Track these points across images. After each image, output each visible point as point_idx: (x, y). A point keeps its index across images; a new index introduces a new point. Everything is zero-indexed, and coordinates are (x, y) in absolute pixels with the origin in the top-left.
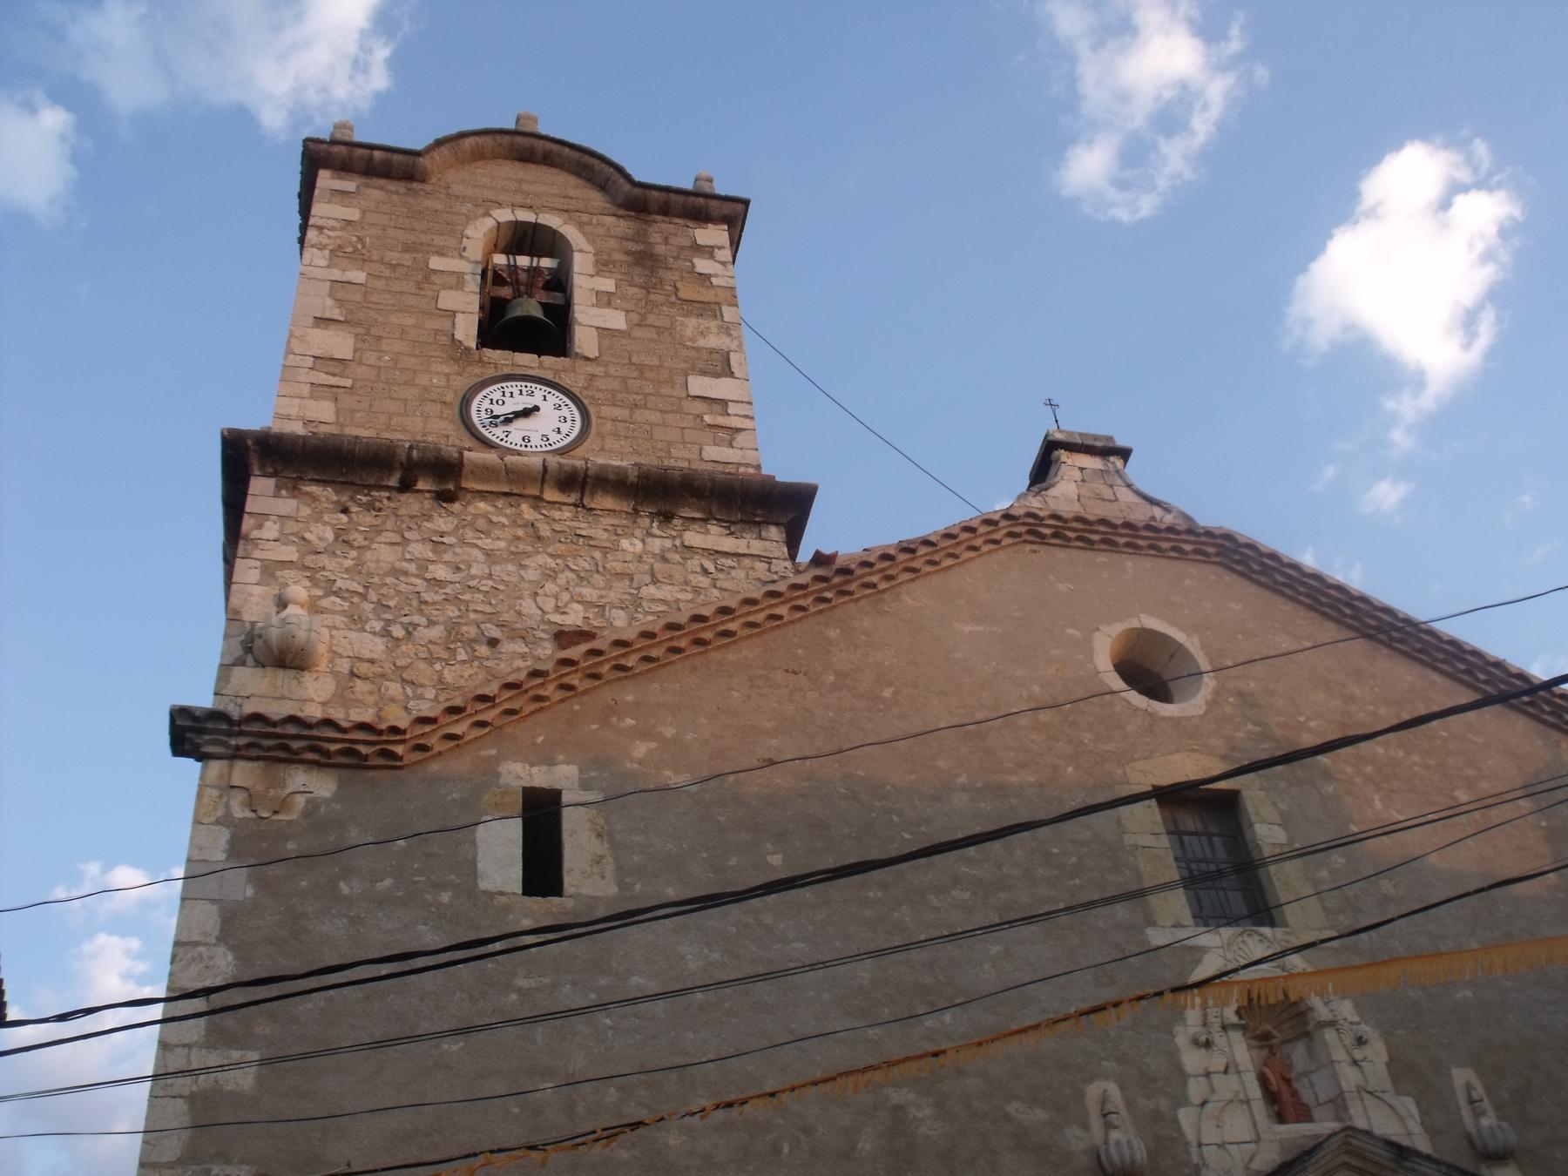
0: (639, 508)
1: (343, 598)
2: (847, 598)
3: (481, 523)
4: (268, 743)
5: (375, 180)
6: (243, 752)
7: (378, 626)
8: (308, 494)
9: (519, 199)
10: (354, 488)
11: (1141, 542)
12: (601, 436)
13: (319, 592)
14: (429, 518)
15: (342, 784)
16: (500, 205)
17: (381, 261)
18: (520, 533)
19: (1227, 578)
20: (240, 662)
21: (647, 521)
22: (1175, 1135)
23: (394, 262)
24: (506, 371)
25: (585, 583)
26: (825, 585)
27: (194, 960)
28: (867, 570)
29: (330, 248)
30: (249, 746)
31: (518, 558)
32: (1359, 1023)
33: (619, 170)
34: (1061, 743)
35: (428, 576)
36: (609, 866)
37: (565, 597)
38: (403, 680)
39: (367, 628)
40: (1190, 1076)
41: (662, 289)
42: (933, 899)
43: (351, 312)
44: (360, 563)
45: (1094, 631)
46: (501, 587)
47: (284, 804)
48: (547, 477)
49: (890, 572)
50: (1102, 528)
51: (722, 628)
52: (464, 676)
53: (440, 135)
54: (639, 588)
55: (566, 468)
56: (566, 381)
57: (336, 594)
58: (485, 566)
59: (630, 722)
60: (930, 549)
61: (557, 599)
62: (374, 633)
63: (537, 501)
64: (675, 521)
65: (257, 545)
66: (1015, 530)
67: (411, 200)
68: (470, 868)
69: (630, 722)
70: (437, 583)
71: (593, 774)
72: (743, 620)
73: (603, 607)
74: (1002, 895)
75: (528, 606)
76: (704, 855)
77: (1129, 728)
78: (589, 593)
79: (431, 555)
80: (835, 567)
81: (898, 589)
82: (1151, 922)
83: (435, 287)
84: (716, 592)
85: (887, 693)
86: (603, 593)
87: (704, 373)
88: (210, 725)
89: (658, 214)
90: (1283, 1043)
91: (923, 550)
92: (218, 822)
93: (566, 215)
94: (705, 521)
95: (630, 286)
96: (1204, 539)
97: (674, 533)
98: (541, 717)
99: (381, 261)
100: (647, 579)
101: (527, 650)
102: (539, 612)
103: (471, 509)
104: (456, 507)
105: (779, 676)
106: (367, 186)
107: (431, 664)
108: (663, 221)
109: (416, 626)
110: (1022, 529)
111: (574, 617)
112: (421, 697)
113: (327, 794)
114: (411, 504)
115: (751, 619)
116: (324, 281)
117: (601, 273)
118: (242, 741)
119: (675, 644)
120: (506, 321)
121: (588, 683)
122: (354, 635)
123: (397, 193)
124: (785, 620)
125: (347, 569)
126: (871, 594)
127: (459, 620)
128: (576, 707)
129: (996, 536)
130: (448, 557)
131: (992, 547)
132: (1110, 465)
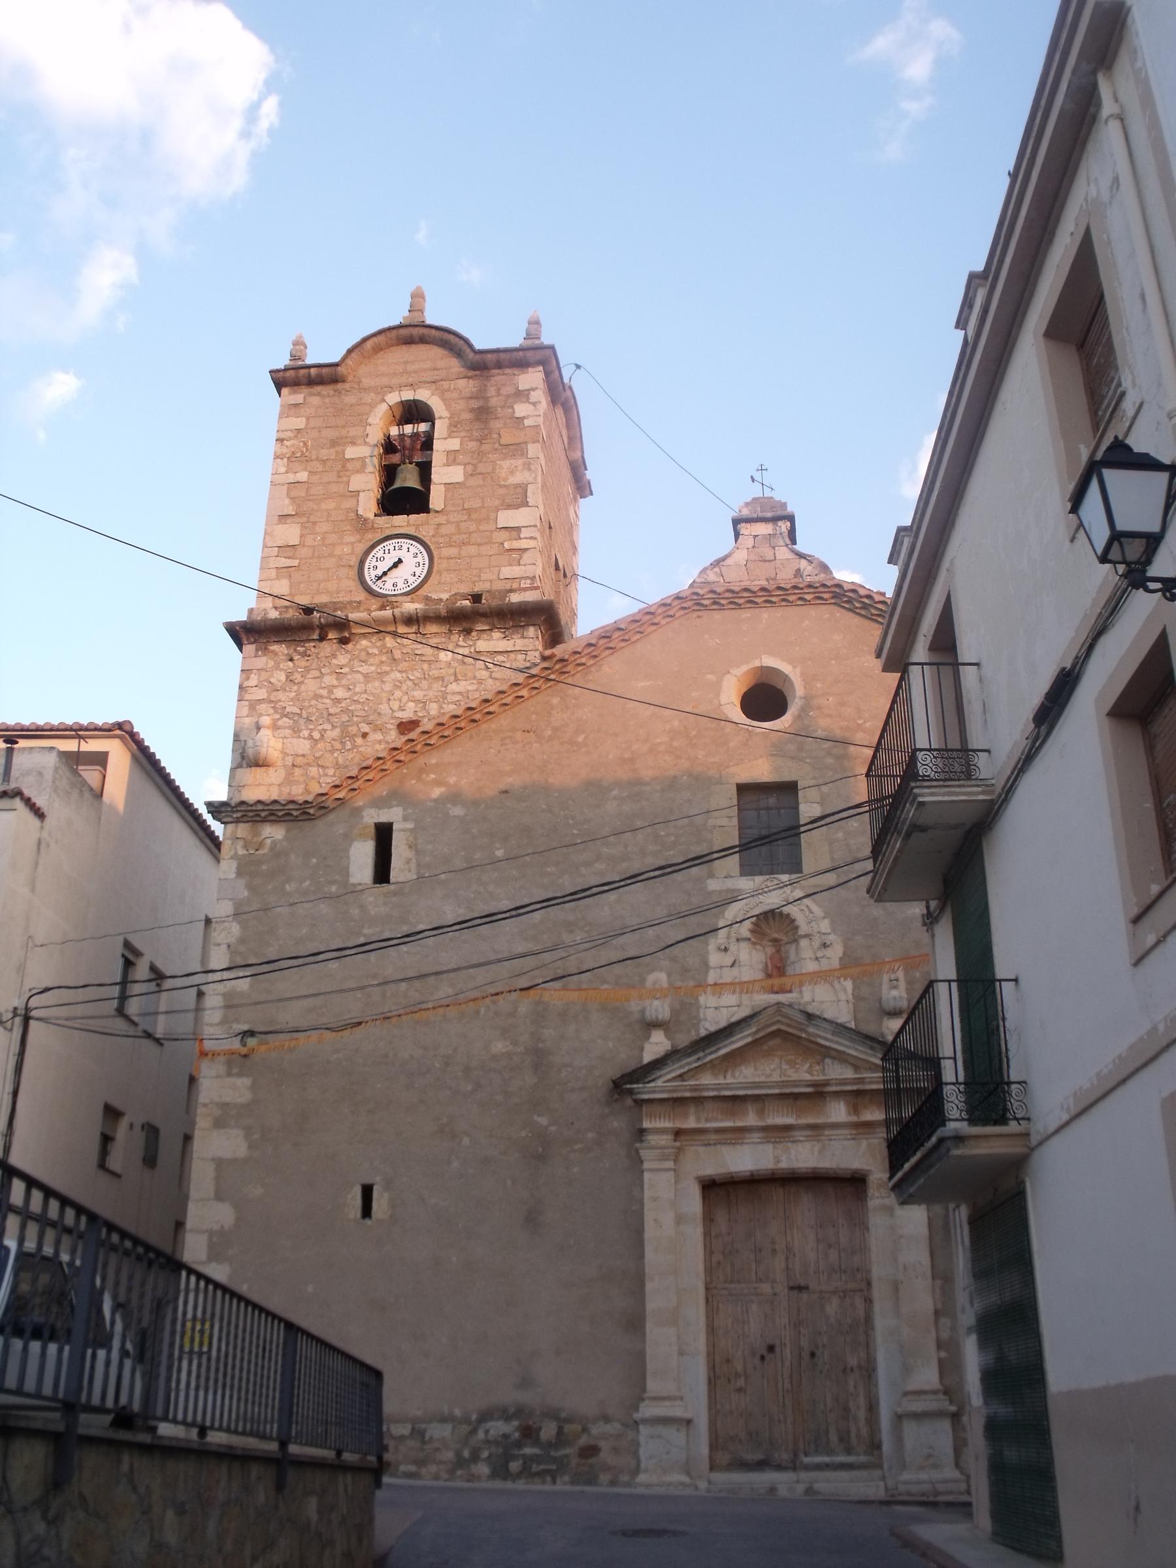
0: (452, 629)
1: (289, 718)
2: (567, 675)
3: (363, 655)
4: (251, 814)
5: (315, 388)
6: (241, 820)
7: (306, 733)
8: (273, 651)
9: (403, 380)
10: (296, 643)
11: (774, 599)
12: (440, 573)
13: (278, 716)
14: (334, 656)
15: (288, 831)
16: (391, 389)
17: (317, 459)
18: (384, 658)
19: (838, 615)
20: (240, 766)
21: (457, 636)
22: (693, 1001)
23: (325, 458)
24: (388, 533)
25: (417, 687)
26: (550, 671)
27: (223, 929)
28: (578, 656)
29: (287, 456)
30: (243, 816)
31: (381, 675)
32: (830, 934)
33: (466, 341)
34: (683, 761)
35: (333, 697)
36: (413, 865)
37: (405, 699)
38: (319, 765)
39: (301, 735)
40: (711, 968)
41: (491, 438)
42: (583, 870)
43: (299, 506)
44: (298, 693)
45: (725, 674)
46: (371, 698)
47: (261, 845)
48: (397, 620)
49: (594, 653)
50: (746, 594)
51: (487, 710)
52: (351, 760)
53: (349, 345)
54: (446, 687)
55: (405, 615)
56: (423, 533)
57: (286, 716)
58: (363, 685)
59: (433, 776)
60: (622, 632)
61: (400, 701)
62: (304, 738)
63: (395, 634)
64: (474, 634)
65: (246, 691)
66: (685, 605)
67: (336, 399)
68: (346, 872)
69: (433, 776)
70: (337, 701)
71: (410, 811)
72: (499, 703)
73: (425, 703)
74: (624, 864)
75: (384, 708)
76: (463, 853)
77: (732, 744)
78: (418, 694)
79: (335, 682)
80: (555, 660)
81: (601, 662)
82: (711, 875)
83: (348, 473)
84: (490, 681)
85: (580, 739)
86: (426, 693)
87: (509, 507)
88: (223, 809)
89: (495, 368)
90: (786, 943)
91: (617, 634)
92: (232, 858)
93: (434, 386)
94: (491, 630)
95: (470, 440)
96: (821, 589)
97: (471, 643)
98: (385, 779)
99: (317, 459)
100: (452, 678)
101: (382, 738)
102: (390, 711)
103: (358, 646)
104: (350, 646)
105: (519, 735)
106: (311, 394)
107: (332, 754)
108: (499, 374)
109: (325, 730)
110: (690, 603)
111: (407, 715)
112: (326, 775)
113: (280, 837)
114: (327, 648)
115: (504, 701)
116: (283, 485)
117: (453, 434)
118: (239, 815)
119: (458, 725)
120: (395, 489)
121: (411, 756)
122: (295, 741)
123: (329, 396)
124: (526, 697)
125: (292, 699)
126: (583, 669)
127: (348, 723)
128: (405, 771)
129: (671, 613)
130: (344, 682)
131: (668, 619)
132: (778, 528)
